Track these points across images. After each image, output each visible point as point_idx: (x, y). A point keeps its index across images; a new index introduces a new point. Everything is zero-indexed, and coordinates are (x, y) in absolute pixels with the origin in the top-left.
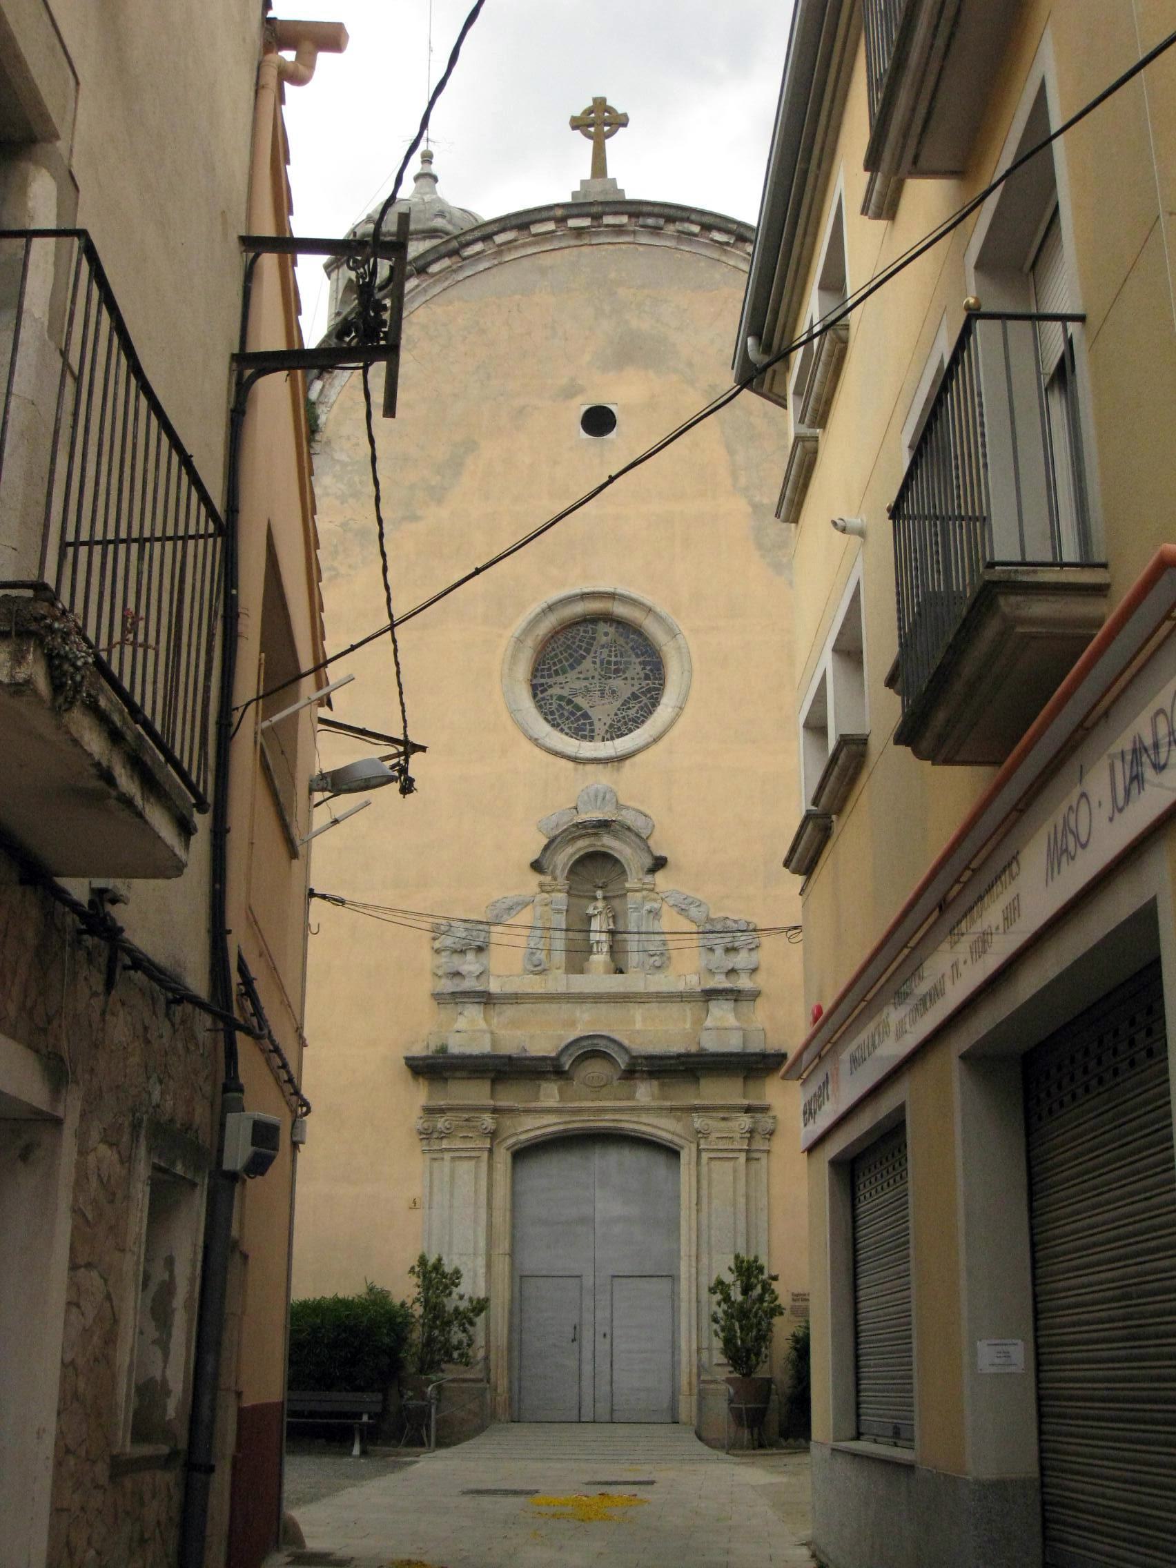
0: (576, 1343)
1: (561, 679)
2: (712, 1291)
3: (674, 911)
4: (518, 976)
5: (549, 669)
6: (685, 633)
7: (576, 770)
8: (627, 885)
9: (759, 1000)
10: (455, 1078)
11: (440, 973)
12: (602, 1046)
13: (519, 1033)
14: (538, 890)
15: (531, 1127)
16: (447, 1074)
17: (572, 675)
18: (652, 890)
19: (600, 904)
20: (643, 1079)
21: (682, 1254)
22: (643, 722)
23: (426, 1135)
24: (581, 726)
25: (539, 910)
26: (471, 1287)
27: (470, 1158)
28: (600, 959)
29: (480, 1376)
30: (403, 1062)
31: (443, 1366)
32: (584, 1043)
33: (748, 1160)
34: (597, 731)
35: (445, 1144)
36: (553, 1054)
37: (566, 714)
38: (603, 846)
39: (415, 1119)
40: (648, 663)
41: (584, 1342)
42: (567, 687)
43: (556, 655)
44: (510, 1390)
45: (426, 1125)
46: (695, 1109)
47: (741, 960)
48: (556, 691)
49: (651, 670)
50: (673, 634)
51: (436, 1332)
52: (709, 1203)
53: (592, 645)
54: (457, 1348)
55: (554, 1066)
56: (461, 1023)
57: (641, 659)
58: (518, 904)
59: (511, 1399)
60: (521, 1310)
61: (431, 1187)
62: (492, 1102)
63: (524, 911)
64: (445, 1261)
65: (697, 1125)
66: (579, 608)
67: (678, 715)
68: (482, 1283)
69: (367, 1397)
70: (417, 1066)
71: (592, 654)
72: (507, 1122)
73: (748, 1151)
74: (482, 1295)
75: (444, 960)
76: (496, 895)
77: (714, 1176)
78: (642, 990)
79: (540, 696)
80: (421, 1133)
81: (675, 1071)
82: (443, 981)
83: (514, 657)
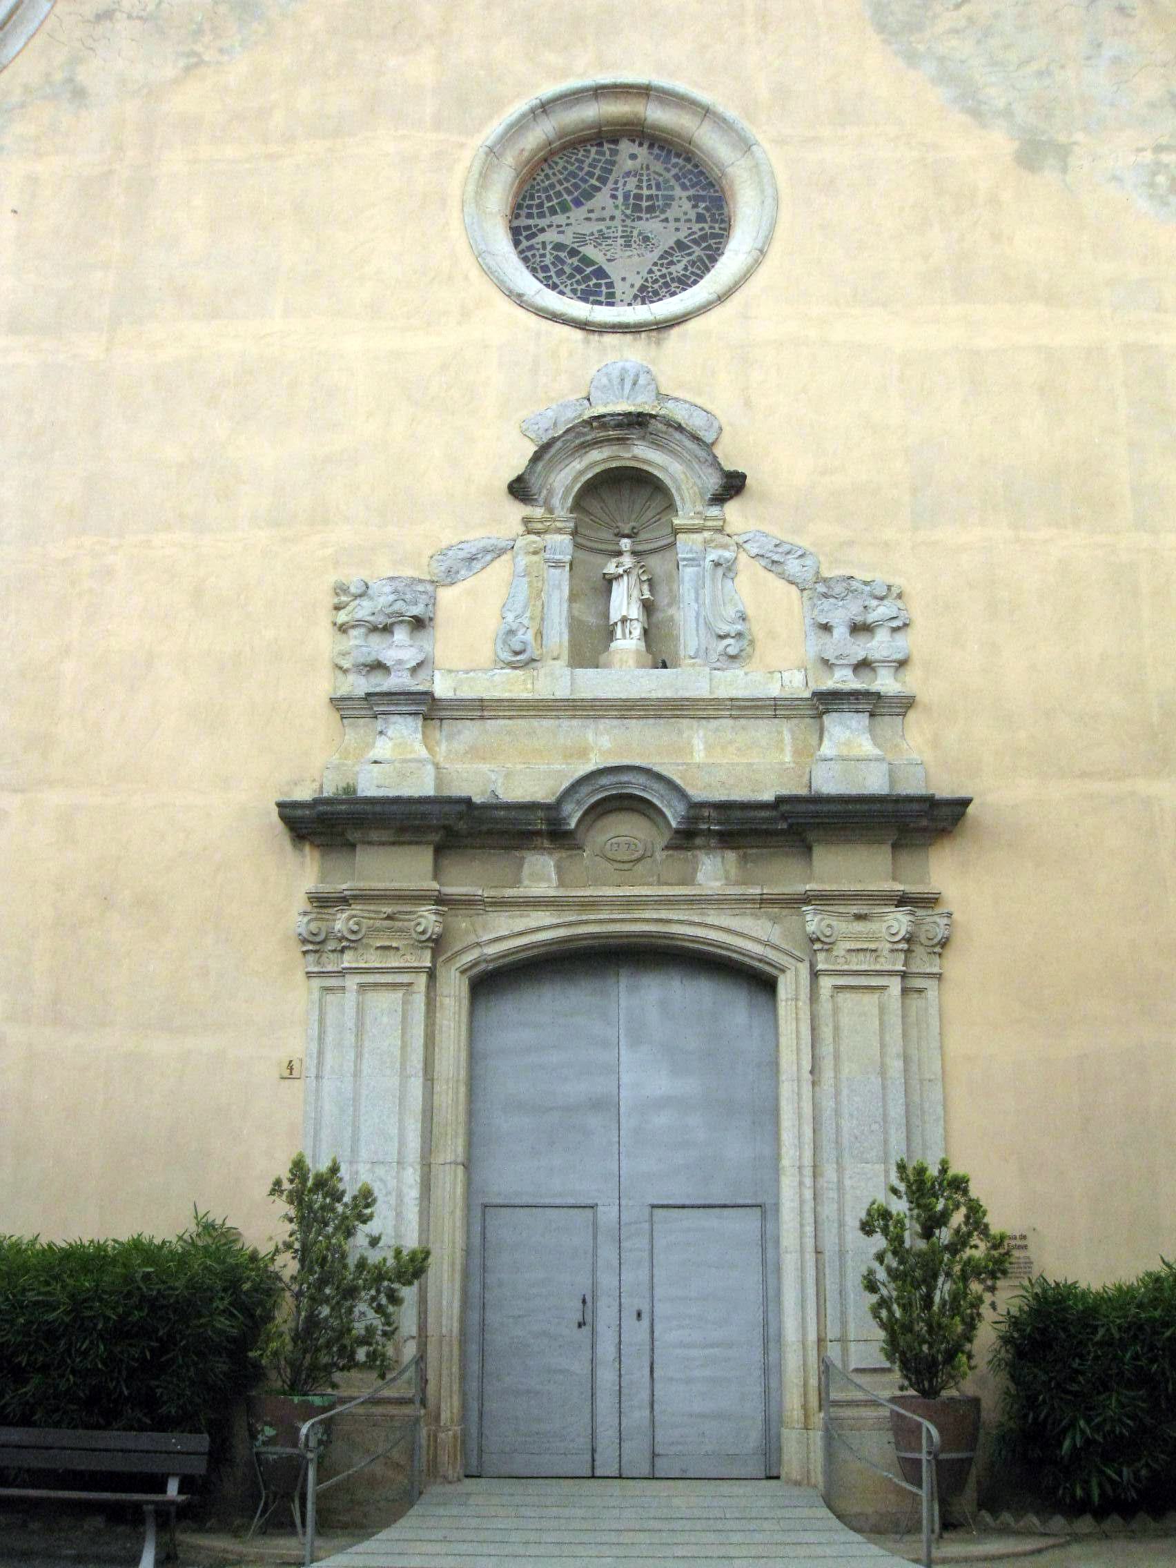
0: (586, 1330)
1: (560, 219)
2: (867, 1228)
3: (757, 566)
4: (485, 670)
5: (541, 205)
6: (766, 145)
7: (587, 342)
8: (676, 521)
9: (912, 715)
10: (370, 843)
11: (346, 664)
12: (636, 786)
13: (485, 767)
14: (521, 529)
15: (504, 933)
16: (353, 835)
17: (577, 214)
18: (720, 530)
19: (627, 561)
20: (707, 848)
21: (786, 1162)
22: (695, 282)
23: (314, 944)
24: (592, 283)
25: (523, 561)
26: (393, 1226)
27: (394, 986)
28: (628, 643)
29: (410, 1393)
30: (275, 811)
31: (337, 1376)
32: (604, 781)
33: (905, 991)
34: (618, 295)
35: (348, 960)
36: (551, 799)
37: (568, 270)
38: (635, 458)
39: (296, 917)
40: (703, 199)
41: (601, 1327)
42: (569, 232)
43: (552, 186)
44: (464, 1418)
45: (313, 927)
46: (807, 899)
47: (879, 645)
48: (551, 236)
49: (707, 209)
50: (745, 145)
51: (325, 1311)
52: (837, 1069)
53: (610, 171)
54: (365, 1341)
55: (550, 821)
56: (383, 748)
57: (691, 192)
58: (486, 551)
59: (465, 1433)
60: (484, 1268)
61: (321, 1039)
62: (435, 886)
63: (496, 564)
64: (344, 1172)
65: (811, 928)
66: (590, 112)
67: (757, 263)
68: (412, 1214)
69: (175, 1441)
70: (301, 819)
71: (610, 185)
72: (462, 923)
73: (904, 975)
74: (411, 1242)
75: (353, 642)
76: (448, 538)
77: (845, 1020)
78: (706, 694)
79: (525, 244)
80: (305, 941)
81: (768, 833)
82: (351, 678)
83: (484, 178)
